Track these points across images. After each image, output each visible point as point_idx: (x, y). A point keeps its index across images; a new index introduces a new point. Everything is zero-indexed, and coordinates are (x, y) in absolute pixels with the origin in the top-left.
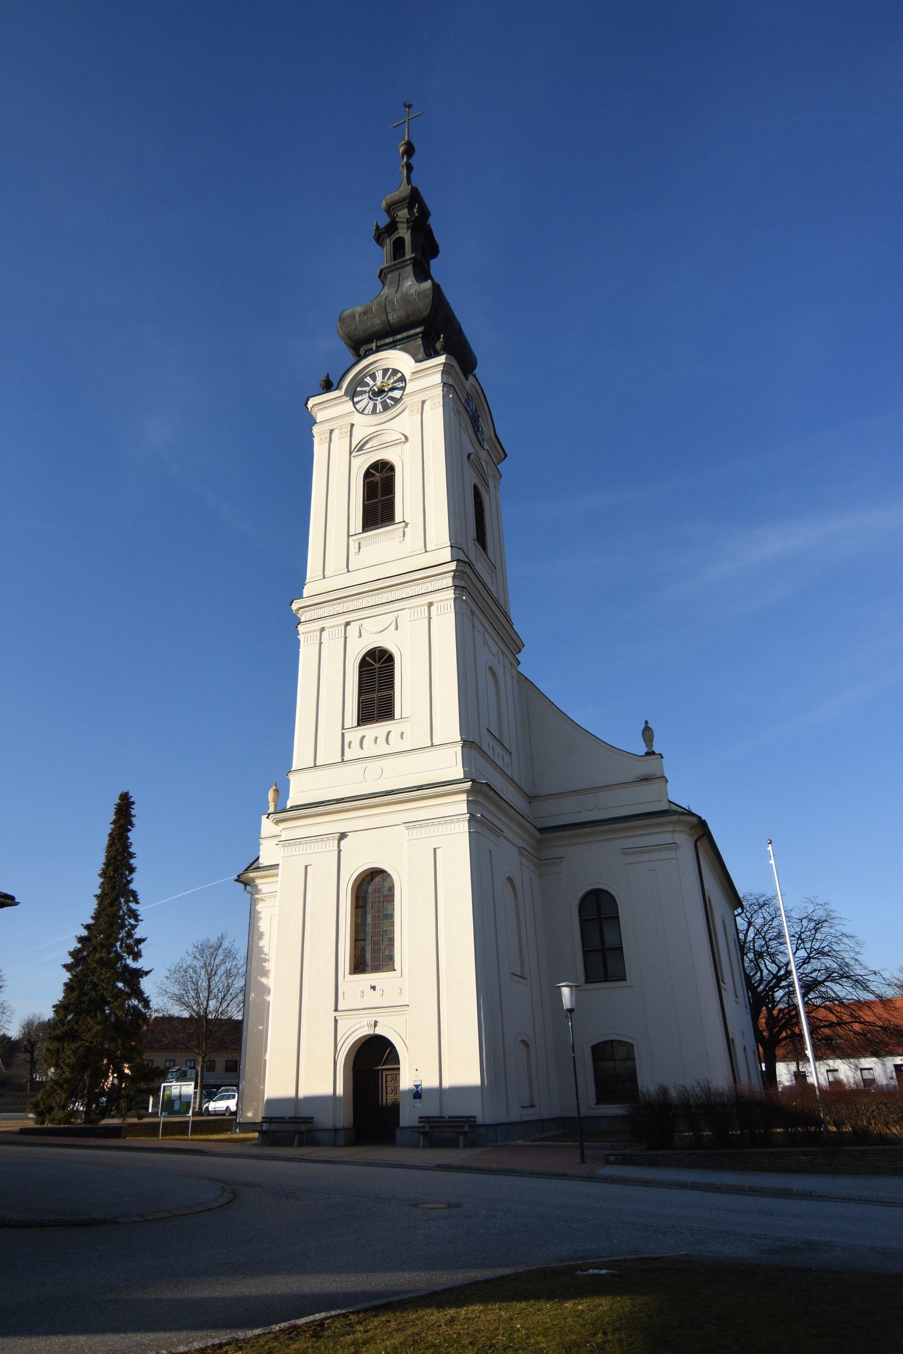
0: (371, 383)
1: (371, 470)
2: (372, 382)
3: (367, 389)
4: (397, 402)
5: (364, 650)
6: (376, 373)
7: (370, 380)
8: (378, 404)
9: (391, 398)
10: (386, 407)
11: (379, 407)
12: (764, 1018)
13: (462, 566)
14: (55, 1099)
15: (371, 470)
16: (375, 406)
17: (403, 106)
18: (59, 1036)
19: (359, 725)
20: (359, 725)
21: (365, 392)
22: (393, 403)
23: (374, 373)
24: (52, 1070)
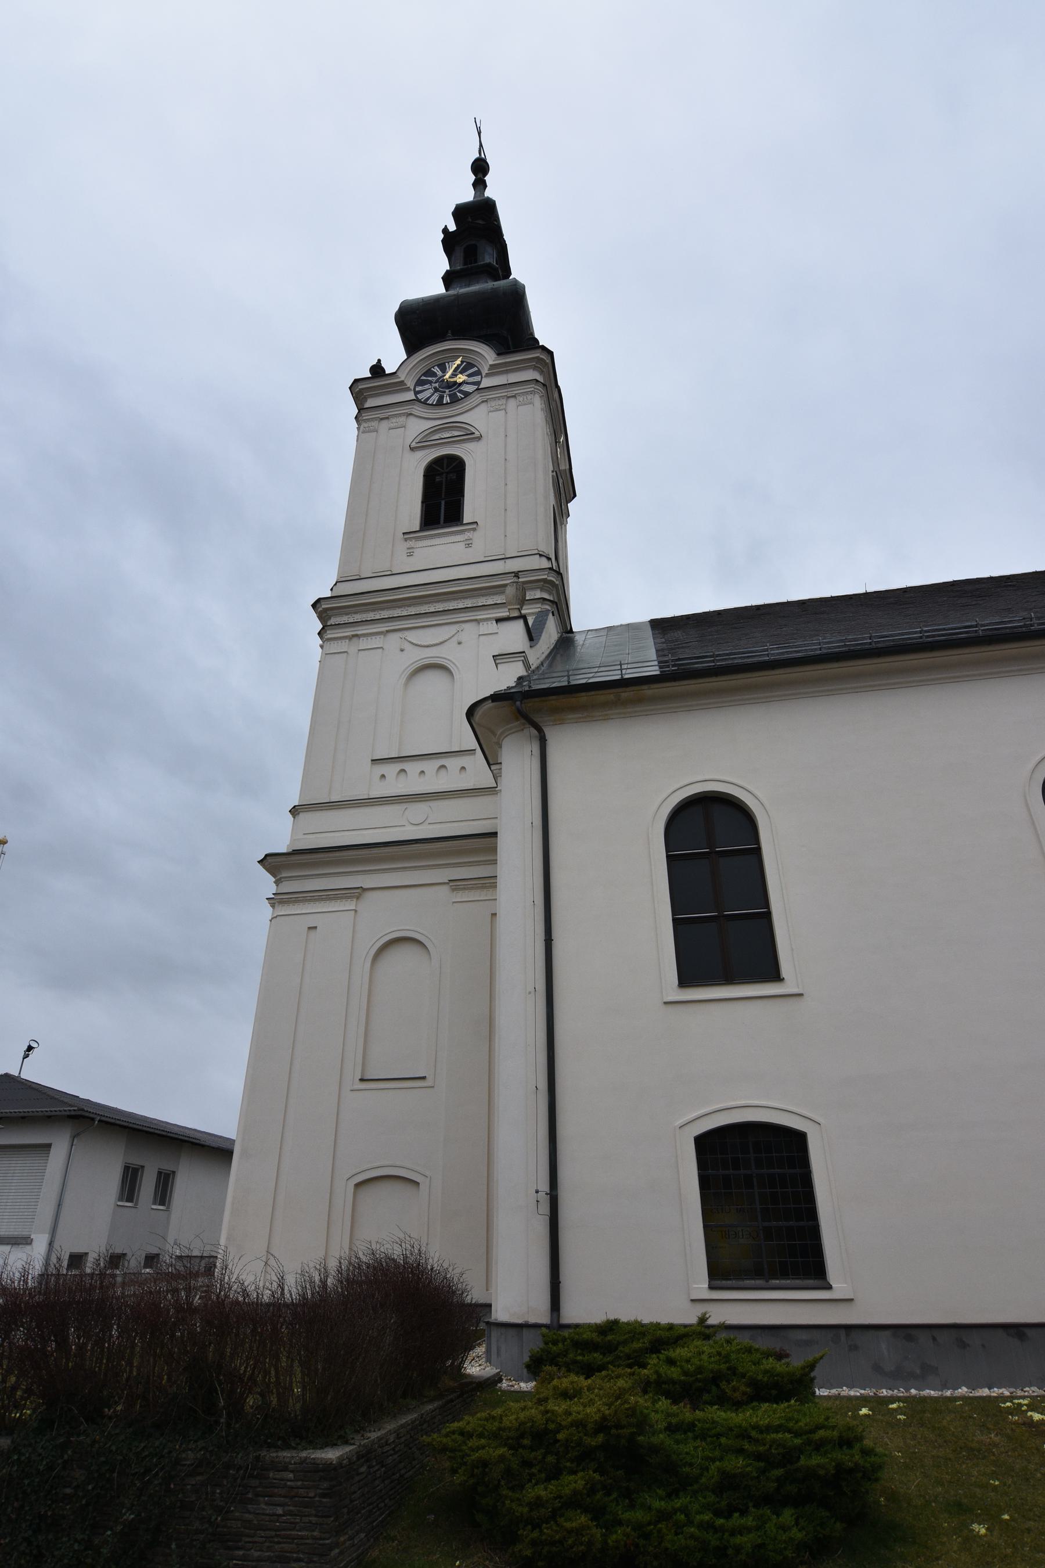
0: (439, 373)
1: (434, 466)
2: (440, 372)
3: (435, 379)
4: (467, 396)
5: (420, 662)
6: (447, 364)
7: (438, 369)
8: (445, 395)
9: (461, 392)
10: (454, 400)
11: (447, 399)
12: (861, 1394)
13: (554, 577)
14: (599, 1400)
15: (434, 466)
16: (441, 398)
17: (425, 771)
18: (475, 1462)
19: (422, 530)
20: (422, 530)
21: (430, 382)
22: (463, 396)
23: (444, 363)
24: (231, 1472)
